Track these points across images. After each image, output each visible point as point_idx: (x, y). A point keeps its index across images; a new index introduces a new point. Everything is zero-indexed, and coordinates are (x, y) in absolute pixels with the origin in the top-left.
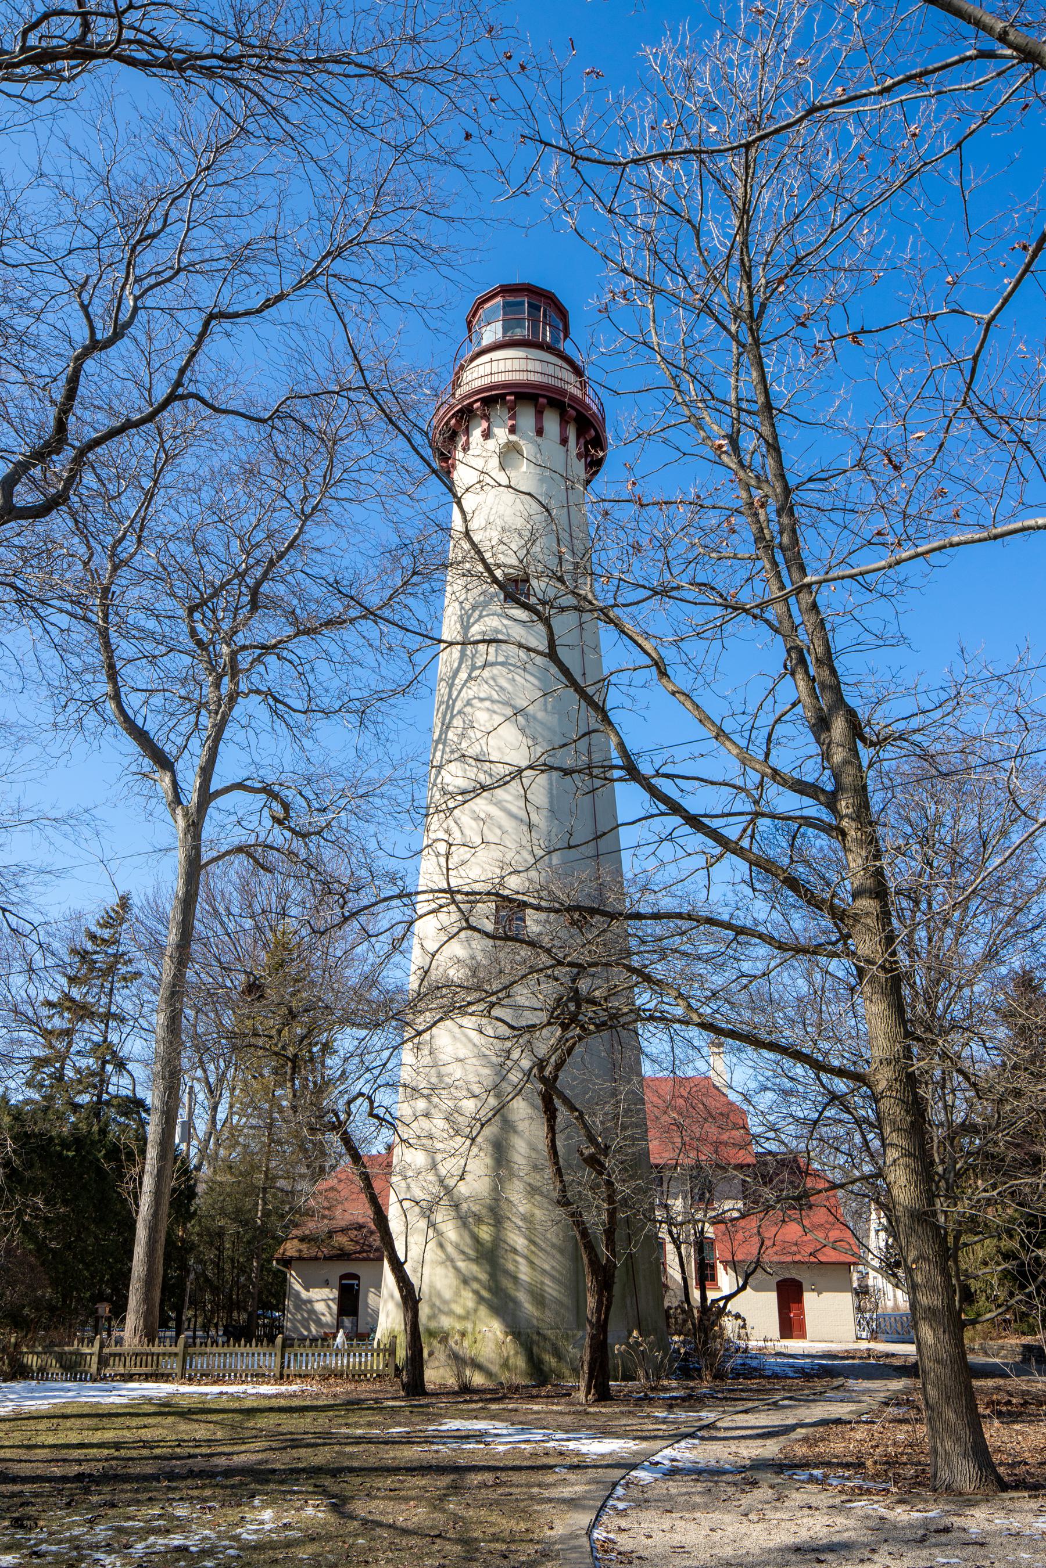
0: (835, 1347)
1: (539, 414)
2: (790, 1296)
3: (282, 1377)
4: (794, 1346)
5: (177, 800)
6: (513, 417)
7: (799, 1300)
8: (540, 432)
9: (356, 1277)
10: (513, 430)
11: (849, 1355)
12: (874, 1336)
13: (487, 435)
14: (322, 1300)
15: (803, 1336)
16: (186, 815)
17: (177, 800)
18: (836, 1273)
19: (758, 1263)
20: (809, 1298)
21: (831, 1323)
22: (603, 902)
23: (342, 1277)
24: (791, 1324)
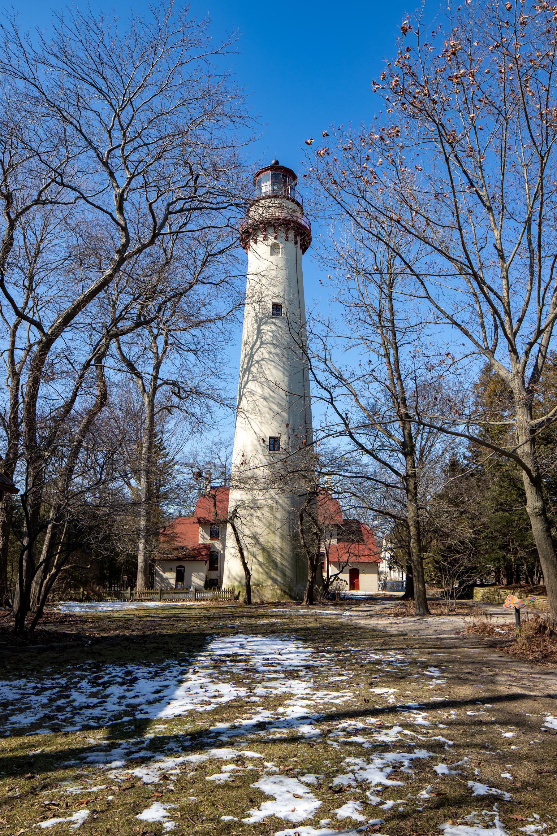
0: (370, 593)
1: (287, 232)
2: (354, 575)
3: (160, 600)
4: (355, 592)
5: (144, 391)
6: (276, 232)
7: (358, 578)
8: (287, 239)
9: (184, 567)
10: (276, 238)
11: (377, 595)
12: (384, 588)
13: (265, 239)
14: (171, 577)
15: (358, 589)
16: (148, 397)
17: (144, 391)
18: (373, 567)
19: (347, 563)
20: (361, 576)
21: (369, 584)
22: (49, 379)
23: (177, 567)
24: (354, 585)
